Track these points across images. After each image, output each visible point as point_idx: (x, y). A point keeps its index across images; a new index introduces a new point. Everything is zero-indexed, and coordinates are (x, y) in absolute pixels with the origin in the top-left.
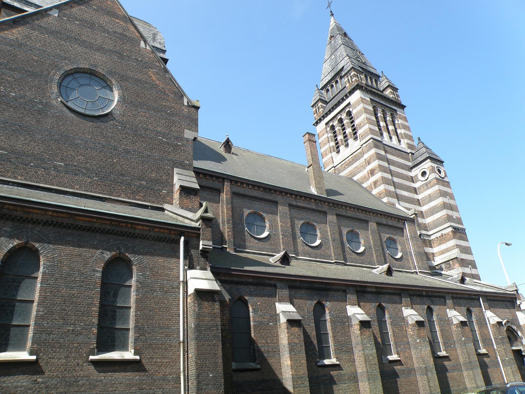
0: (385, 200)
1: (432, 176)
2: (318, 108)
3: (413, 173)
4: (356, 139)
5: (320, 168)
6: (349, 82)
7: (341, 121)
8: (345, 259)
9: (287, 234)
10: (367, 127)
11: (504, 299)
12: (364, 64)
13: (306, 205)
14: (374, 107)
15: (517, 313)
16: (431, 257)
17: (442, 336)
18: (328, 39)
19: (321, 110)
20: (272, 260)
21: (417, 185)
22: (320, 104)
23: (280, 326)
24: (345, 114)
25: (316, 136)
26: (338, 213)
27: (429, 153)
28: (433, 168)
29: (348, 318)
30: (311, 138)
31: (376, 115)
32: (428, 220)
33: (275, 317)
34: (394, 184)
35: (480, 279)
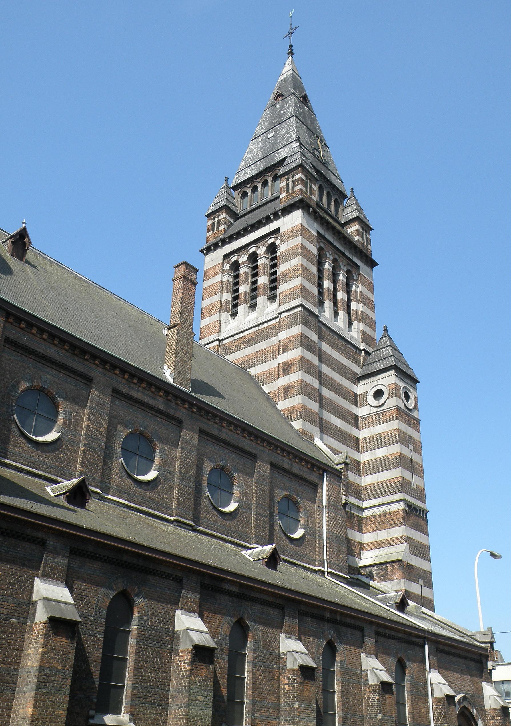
0: (297, 425)
1: (391, 403)
2: (218, 221)
3: (360, 388)
4: (272, 298)
5: (191, 334)
6: (288, 191)
7: (254, 258)
8: (196, 519)
9: (96, 445)
10: (298, 282)
11: (466, 654)
12: (324, 164)
13: (146, 399)
14: (320, 250)
15: (484, 684)
16: (356, 549)
17: (344, 703)
18: (272, 98)
19: (222, 227)
20: (50, 490)
21: (362, 412)
22: (223, 216)
23: (31, 627)
24: (265, 248)
25: (200, 274)
26: (205, 427)
27: (396, 359)
28: (397, 388)
29: (174, 636)
30: (189, 275)
31: (320, 265)
32: (367, 481)
33: (26, 607)
34: (321, 400)
35: (433, 609)
